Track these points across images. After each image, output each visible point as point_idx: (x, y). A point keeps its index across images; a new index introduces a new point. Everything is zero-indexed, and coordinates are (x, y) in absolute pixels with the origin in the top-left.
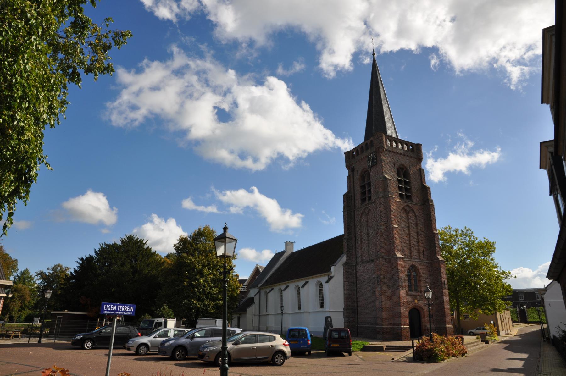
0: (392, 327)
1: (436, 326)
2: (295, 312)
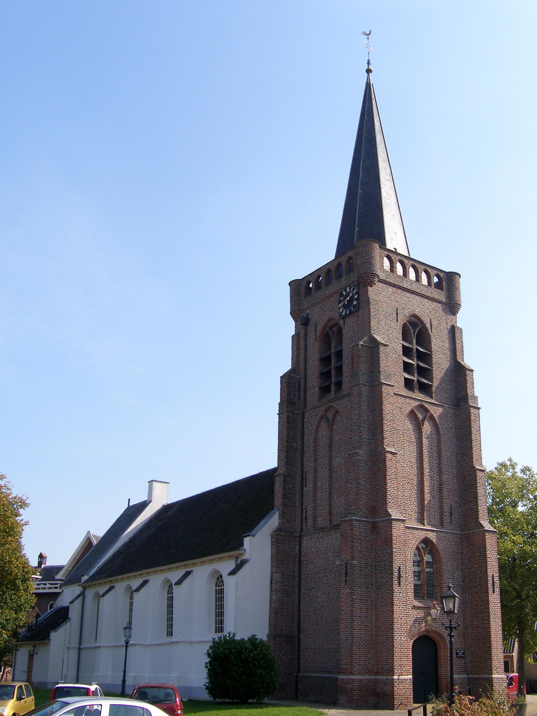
0: (372, 677)
1: (470, 676)
2: (159, 642)
